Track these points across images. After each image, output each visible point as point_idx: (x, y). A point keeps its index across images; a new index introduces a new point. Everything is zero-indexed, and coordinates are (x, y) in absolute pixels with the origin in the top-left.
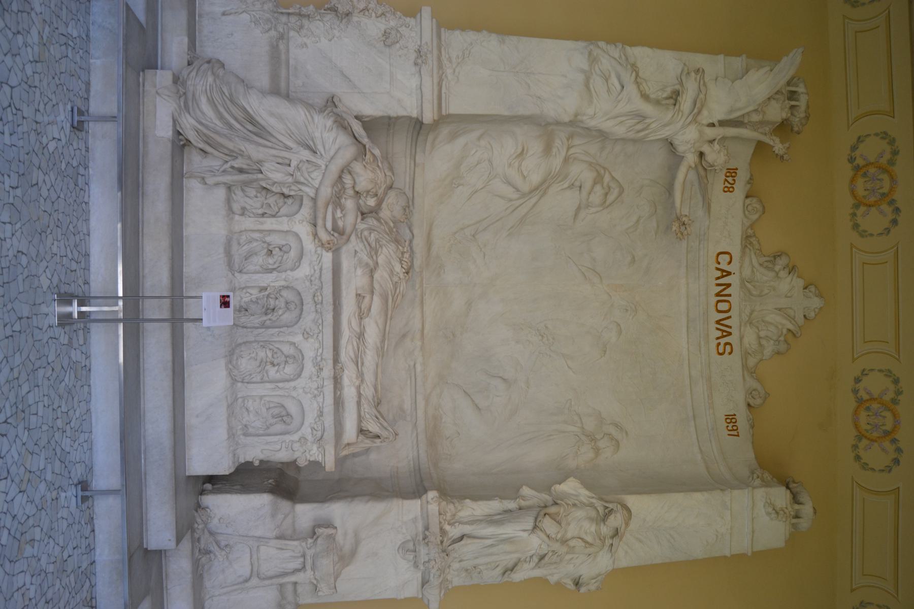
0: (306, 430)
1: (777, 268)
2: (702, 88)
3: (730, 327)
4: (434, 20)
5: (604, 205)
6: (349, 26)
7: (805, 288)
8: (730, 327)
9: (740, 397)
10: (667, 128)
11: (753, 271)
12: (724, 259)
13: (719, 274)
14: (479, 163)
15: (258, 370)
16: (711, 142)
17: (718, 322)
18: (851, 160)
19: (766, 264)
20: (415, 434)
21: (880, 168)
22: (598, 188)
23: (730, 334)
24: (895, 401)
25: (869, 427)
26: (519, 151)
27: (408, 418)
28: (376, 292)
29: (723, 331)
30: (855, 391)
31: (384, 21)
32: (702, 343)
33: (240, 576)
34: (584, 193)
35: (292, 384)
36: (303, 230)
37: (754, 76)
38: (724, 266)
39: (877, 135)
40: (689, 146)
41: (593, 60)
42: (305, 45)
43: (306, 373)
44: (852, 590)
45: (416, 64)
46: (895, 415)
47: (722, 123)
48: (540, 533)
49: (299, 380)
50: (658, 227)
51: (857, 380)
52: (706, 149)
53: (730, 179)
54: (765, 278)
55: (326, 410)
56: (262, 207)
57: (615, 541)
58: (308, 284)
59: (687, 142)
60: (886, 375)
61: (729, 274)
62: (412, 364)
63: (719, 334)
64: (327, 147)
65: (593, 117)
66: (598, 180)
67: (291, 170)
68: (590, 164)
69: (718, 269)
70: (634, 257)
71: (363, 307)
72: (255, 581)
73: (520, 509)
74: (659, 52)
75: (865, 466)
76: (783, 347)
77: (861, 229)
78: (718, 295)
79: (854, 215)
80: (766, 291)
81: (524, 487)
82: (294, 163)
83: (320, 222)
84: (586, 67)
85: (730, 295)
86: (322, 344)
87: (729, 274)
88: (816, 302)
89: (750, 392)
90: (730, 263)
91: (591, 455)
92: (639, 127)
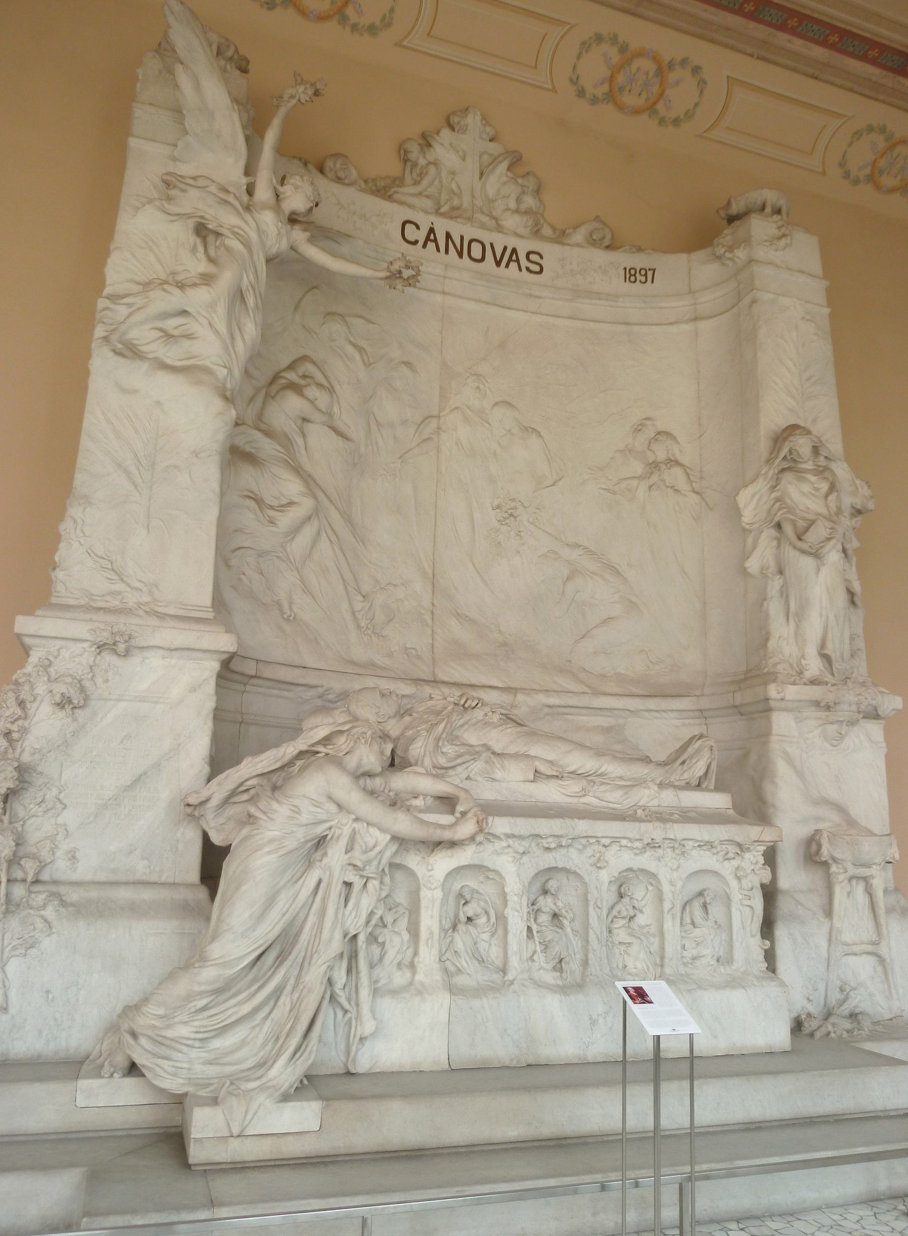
0: (727, 869)
2: (201, 182)
3: (505, 248)
4: (39, 612)
6: (40, 769)
7: (453, 129)
8: (505, 248)
9: (600, 257)
11: (428, 197)
13: (431, 245)
14: (262, 574)
15: (645, 941)
17: (498, 264)
19: (414, 175)
20: (646, 714)
23: (514, 251)
24: (623, 49)
25: (644, 95)
26: (252, 504)
27: (621, 721)
28: (523, 749)
29: (510, 260)
30: (594, 101)
31: (35, 705)
33: (875, 972)
34: (316, 416)
35: (666, 888)
36: (443, 863)
38: (421, 235)
42: (73, 857)
43: (652, 866)
44: (824, 173)
45: (127, 654)
46: (640, 54)
47: (249, 171)
48: (825, 550)
49: (661, 877)
50: (361, 317)
51: (581, 93)
55: (706, 837)
56: (398, 934)
57: (823, 452)
58: (525, 859)
59: (279, 233)
60: (587, 51)
61: (432, 230)
62: (546, 710)
63: (513, 265)
64: (324, 817)
67: (358, 883)
68: (267, 395)
69: (425, 246)
71: (550, 773)
72: (883, 950)
73: (781, 572)
74: (119, 239)
75: (690, 115)
76: (531, 183)
77: (378, 23)
78: (460, 255)
79: (355, 27)
81: (747, 565)
82: (351, 877)
83: (438, 835)
85: (462, 238)
86: (615, 840)
87: (432, 230)
88: (473, 121)
89: (593, 242)
90: (418, 227)
91: (677, 471)
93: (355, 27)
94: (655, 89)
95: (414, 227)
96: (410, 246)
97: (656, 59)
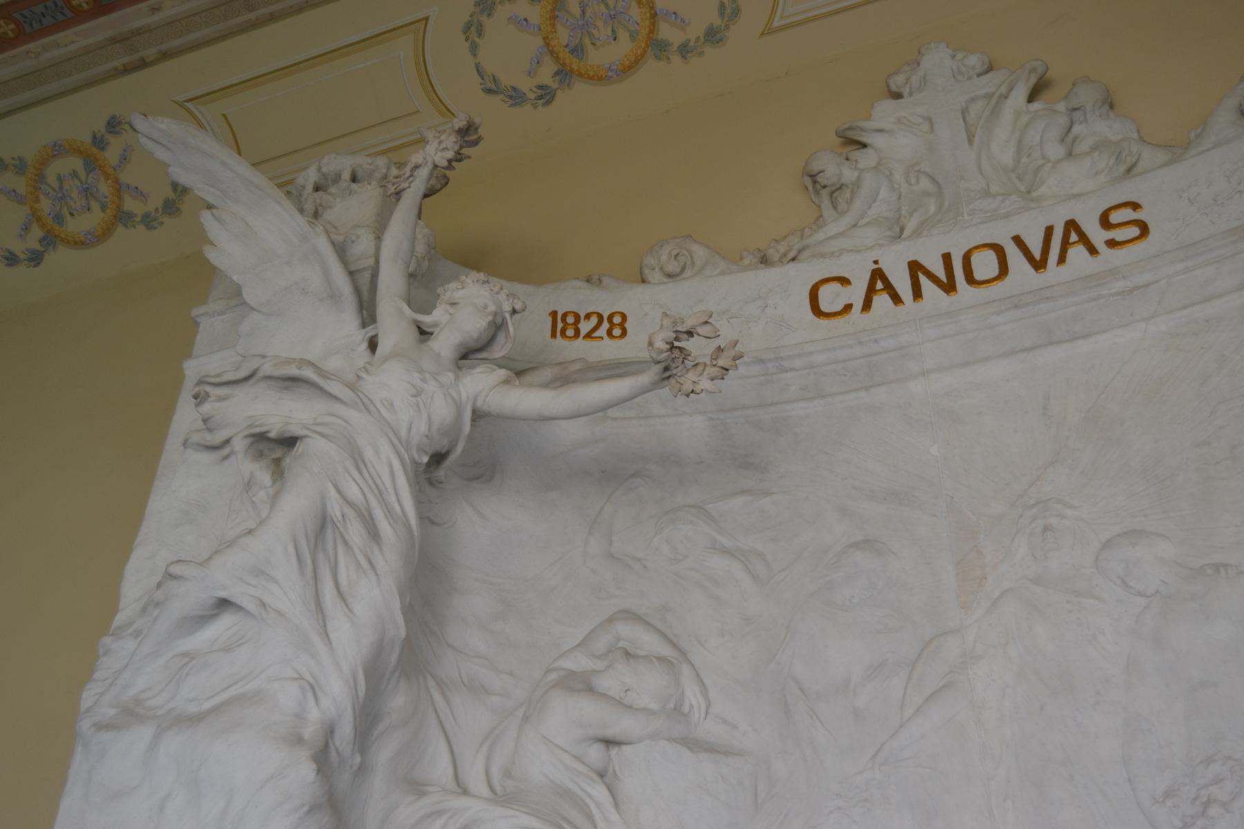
1: (849, 175)
3: (1049, 231)
5: (676, 657)
7: (898, 96)
10: (369, 454)
12: (830, 298)
13: (882, 300)
16: (424, 333)
18: (546, 95)
21: (553, 18)
22: (608, 683)
32: (1119, 285)
37: (228, 250)
39: (474, 49)
40: (431, 386)
41: (132, 714)
47: (367, 312)
50: (743, 492)
52: (445, 344)
53: (585, 327)
54: (884, 193)
61: (878, 274)
63: (1077, 253)
65: (314, 689)
66: (582, 684)
69: (867, 305)
70: (856, 545)
77: (717, 22)
78: (949, 287)
79: (685, 50)
80: (925, 184)
84: (144, 733)
85: (947, 258)
87: (878, 274)
88: (938, 61)
90: (844, 281)
92: (355, 532)
93: (685, 50)
94: (104, 188)
95: (835, 286)
96: (846, 318)
97: (75, 150)
